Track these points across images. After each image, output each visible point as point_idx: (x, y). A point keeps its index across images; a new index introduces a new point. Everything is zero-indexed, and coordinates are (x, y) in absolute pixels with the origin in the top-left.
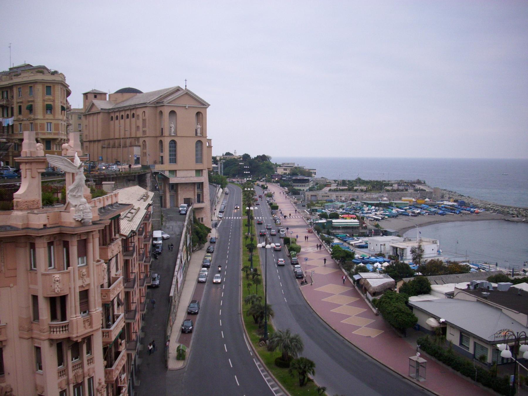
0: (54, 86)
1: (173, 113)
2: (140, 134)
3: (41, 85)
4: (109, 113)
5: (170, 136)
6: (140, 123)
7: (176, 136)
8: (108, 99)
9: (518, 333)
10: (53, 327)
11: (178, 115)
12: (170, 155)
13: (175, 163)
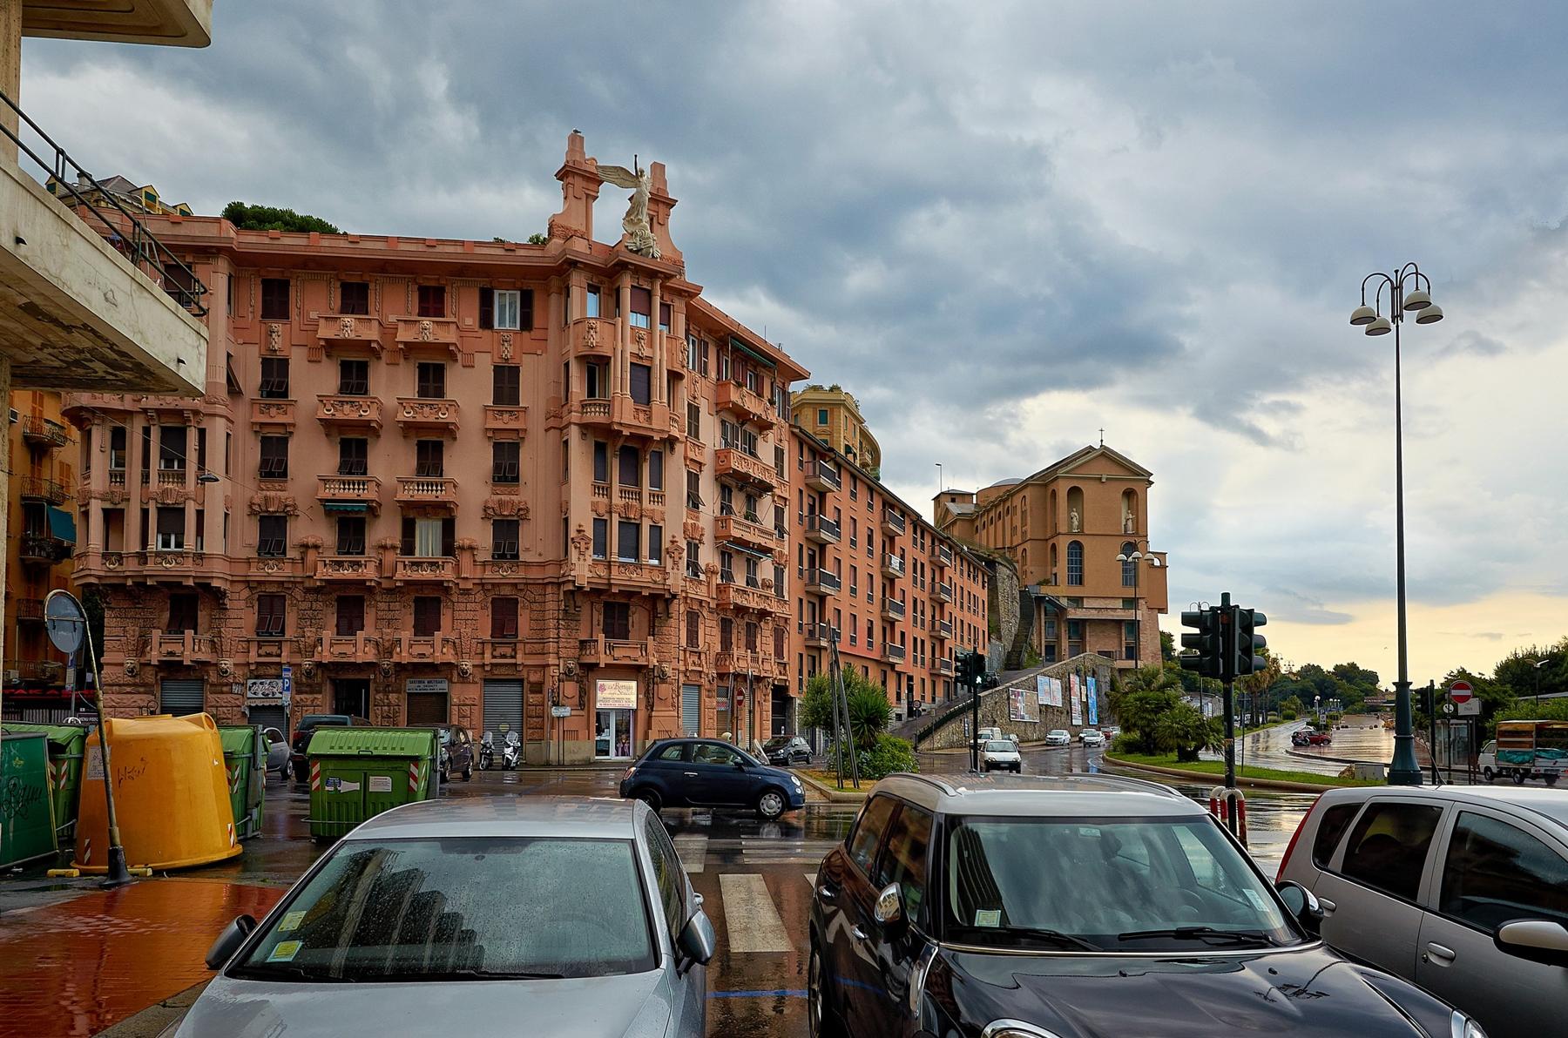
0: (832, 410)
1: (1075, 492)
2: (1017, 540)
3: (811, 410)
4: (972, 521)
5: (1070, 534)
6: (1018, 521)
7: (1081, 533)
8: (975, 502)
9: (1397, 271)
10: (586, 405)
11: (1085, 496)
12: (1070, 570)
13: (1081, 583)
